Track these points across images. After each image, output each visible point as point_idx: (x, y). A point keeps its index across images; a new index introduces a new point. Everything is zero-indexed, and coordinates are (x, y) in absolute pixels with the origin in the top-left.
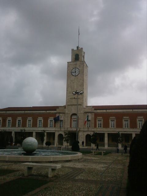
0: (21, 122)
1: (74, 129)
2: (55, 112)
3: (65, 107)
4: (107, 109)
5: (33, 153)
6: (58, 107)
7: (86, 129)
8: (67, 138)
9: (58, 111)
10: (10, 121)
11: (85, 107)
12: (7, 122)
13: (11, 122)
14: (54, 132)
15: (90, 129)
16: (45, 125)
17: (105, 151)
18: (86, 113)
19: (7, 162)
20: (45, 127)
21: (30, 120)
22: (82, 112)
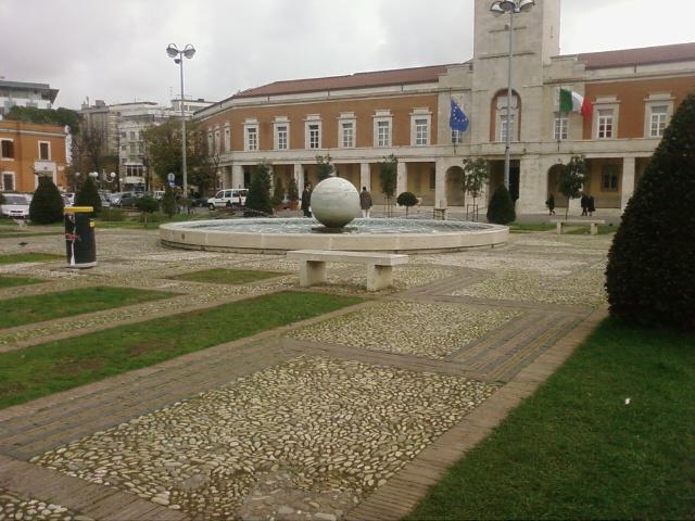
0: (320, 130)
1: (501, 149)
2: (434, 86)
3: (471, 67)
4: (640, 64)
5: (348, 226)
6: (443, 69)
7: (552, 147)
8: (473, 180)
9: (444, 82)
10: (284, 128)
11: (549, 62)
12: (276, 133)
13: (288, 131)
14: (432, 160)
15: (565, 147)
16: (402, 138)
17: (603, 222)
18: (552, 83)
19: (262, 251)
20: (401, 145)
21: (350, 122)
22: (537, 80)
